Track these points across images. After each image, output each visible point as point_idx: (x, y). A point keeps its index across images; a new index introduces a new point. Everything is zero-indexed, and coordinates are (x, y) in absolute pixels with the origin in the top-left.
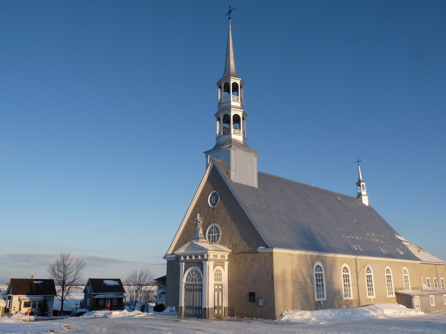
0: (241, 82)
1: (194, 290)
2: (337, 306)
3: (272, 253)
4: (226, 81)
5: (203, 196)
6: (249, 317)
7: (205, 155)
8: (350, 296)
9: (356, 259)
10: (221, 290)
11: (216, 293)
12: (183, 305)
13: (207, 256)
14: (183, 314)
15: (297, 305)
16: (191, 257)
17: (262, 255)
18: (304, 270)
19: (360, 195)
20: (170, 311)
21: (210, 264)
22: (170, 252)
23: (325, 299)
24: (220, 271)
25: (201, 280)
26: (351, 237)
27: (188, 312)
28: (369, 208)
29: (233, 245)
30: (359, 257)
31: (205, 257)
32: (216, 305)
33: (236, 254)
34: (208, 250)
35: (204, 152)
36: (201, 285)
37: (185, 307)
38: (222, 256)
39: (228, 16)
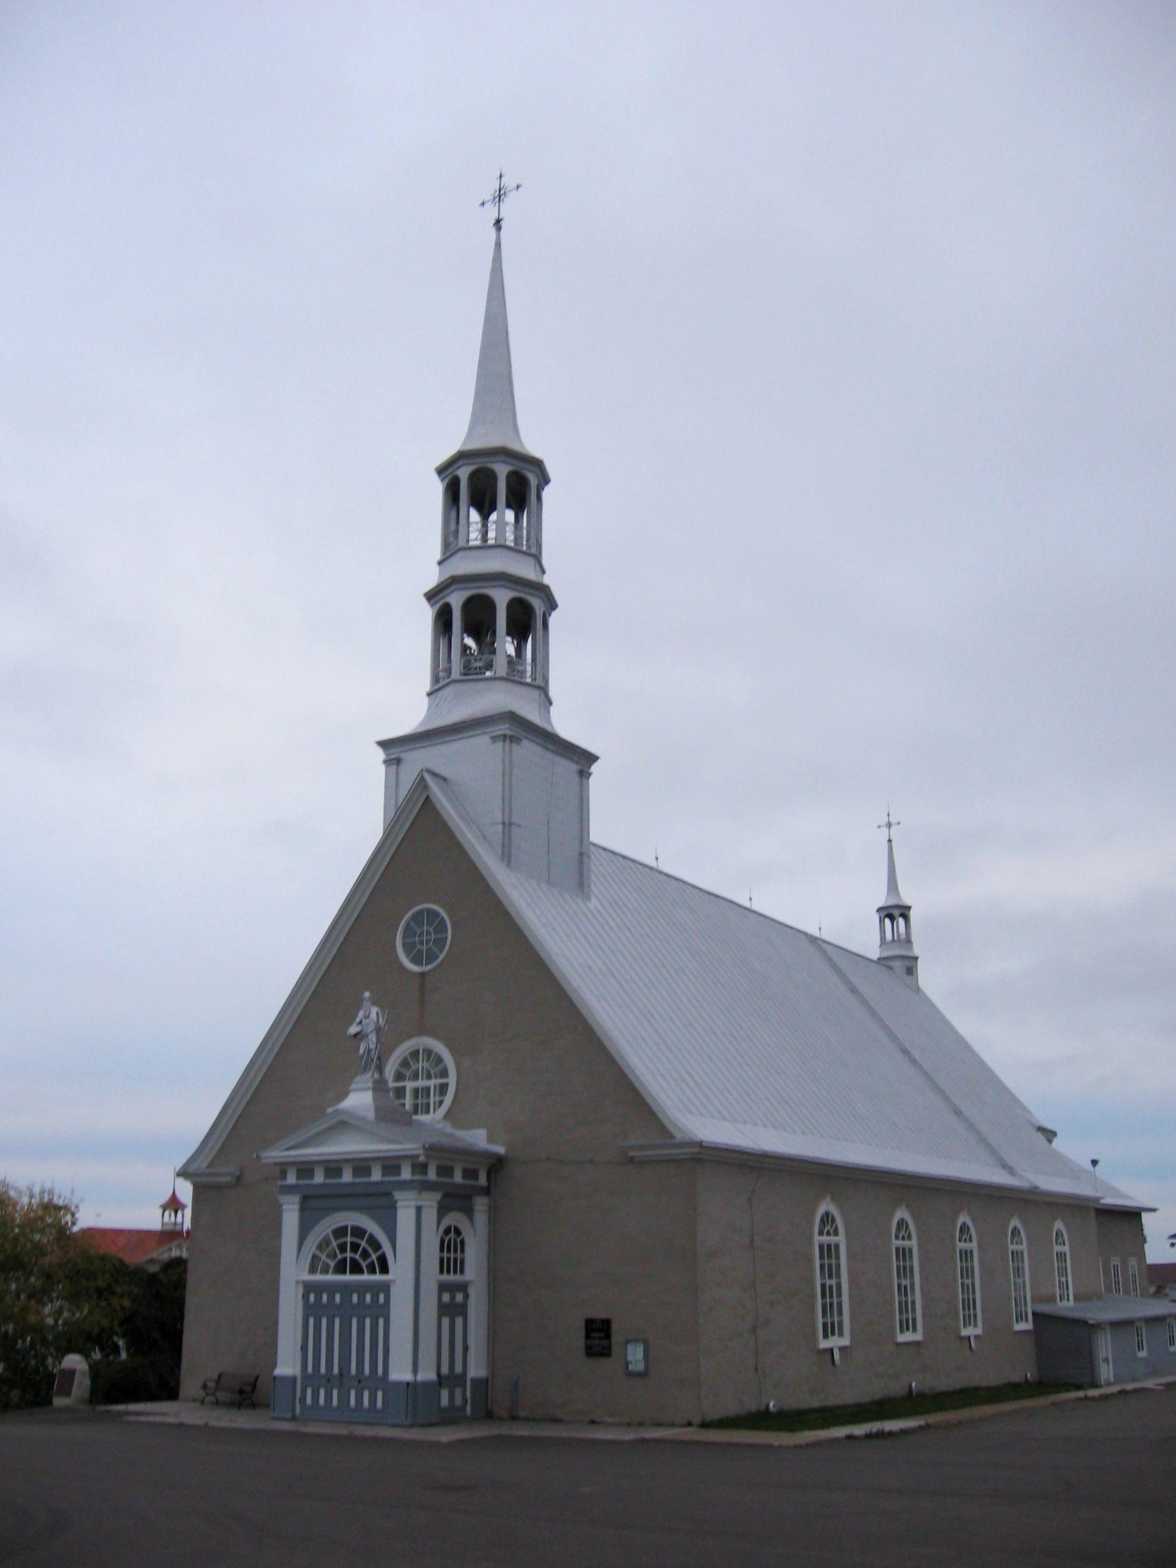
7: (380, 755)
24: (458, 1232)
32: (445, 1370)
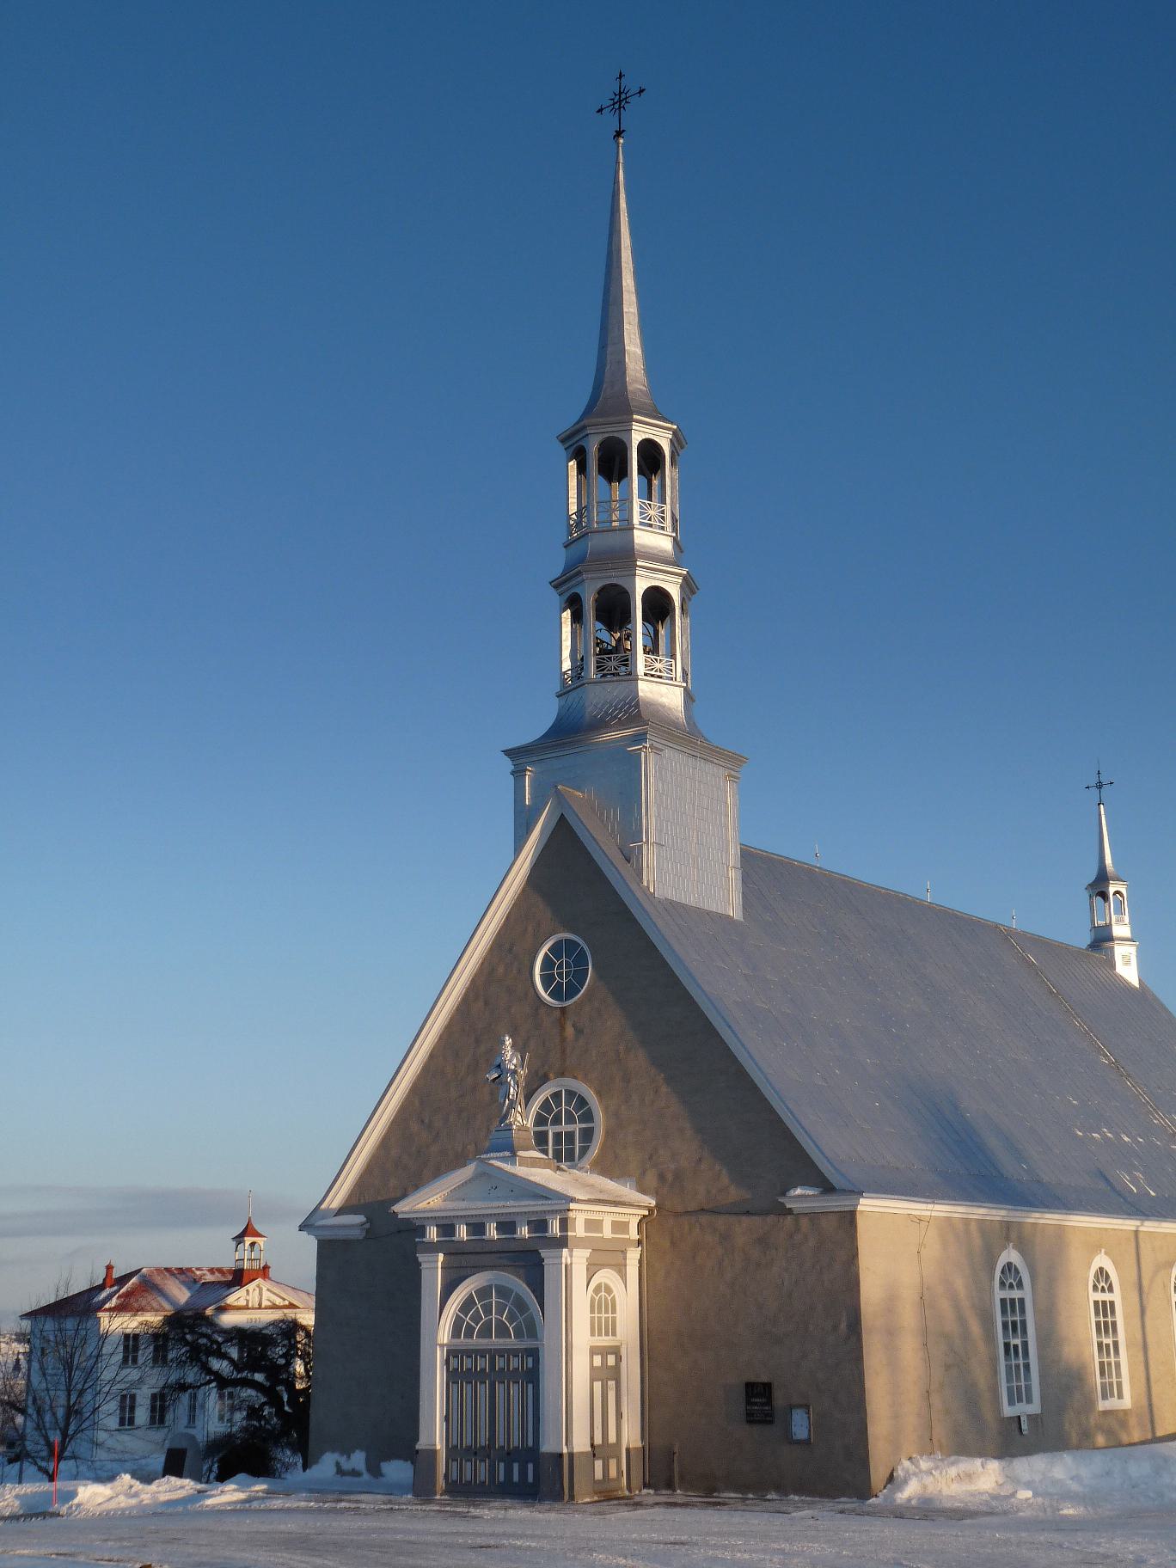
0: (677, 442)
1: (494, 1376)
2: (1074, 1439)
3: (849, 1218)
4: (610, 431)
5: (509, 950)
6: (743, 1487)
7: (508, 765)
8: (1120, 1396)
9: (1136, 1232)
10: (615, 1373)
11: (598, 1385)
12: (439, 1445)
13: (564, 1224)
14: (441, 1482)
15: (940, 1431)
16: (477, 1228)
17: (804, 1222)
18: (960, 1284)
19: (1102, 939)
20: (340, 1471)
21: (576, 1259)
22: (336, 1200)
23: (1035, 1408)
24: (608, 1290)
25: (530, 1329)
26: (1104, 1136)
27: (468, 1476)
28: (1141, 998)
29: (662, 1177)
30: (1149, 1226)
31: (555, 1228)
32: (598, 1440)
33: (677, 1215)
34: (573, 1200)
35: (508, 753)
36: (534, 1353)
37: (452, 1451)
38: (620, 1227)
39: (610, 121)
